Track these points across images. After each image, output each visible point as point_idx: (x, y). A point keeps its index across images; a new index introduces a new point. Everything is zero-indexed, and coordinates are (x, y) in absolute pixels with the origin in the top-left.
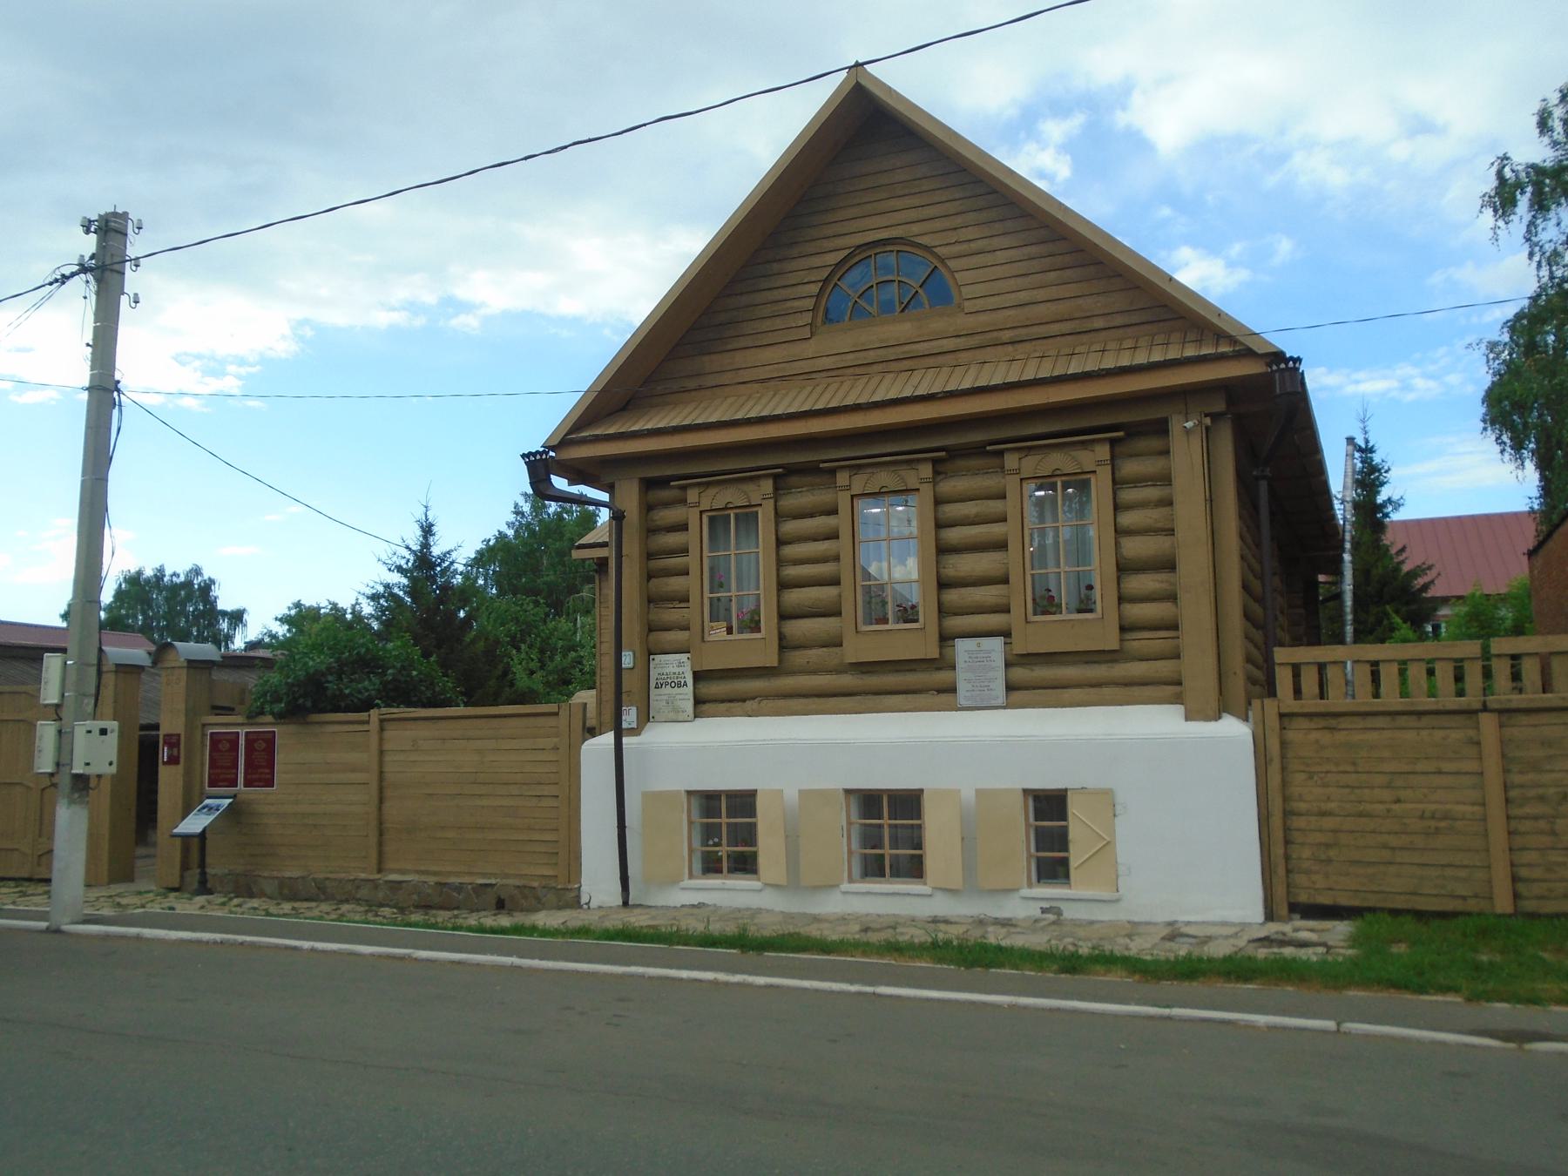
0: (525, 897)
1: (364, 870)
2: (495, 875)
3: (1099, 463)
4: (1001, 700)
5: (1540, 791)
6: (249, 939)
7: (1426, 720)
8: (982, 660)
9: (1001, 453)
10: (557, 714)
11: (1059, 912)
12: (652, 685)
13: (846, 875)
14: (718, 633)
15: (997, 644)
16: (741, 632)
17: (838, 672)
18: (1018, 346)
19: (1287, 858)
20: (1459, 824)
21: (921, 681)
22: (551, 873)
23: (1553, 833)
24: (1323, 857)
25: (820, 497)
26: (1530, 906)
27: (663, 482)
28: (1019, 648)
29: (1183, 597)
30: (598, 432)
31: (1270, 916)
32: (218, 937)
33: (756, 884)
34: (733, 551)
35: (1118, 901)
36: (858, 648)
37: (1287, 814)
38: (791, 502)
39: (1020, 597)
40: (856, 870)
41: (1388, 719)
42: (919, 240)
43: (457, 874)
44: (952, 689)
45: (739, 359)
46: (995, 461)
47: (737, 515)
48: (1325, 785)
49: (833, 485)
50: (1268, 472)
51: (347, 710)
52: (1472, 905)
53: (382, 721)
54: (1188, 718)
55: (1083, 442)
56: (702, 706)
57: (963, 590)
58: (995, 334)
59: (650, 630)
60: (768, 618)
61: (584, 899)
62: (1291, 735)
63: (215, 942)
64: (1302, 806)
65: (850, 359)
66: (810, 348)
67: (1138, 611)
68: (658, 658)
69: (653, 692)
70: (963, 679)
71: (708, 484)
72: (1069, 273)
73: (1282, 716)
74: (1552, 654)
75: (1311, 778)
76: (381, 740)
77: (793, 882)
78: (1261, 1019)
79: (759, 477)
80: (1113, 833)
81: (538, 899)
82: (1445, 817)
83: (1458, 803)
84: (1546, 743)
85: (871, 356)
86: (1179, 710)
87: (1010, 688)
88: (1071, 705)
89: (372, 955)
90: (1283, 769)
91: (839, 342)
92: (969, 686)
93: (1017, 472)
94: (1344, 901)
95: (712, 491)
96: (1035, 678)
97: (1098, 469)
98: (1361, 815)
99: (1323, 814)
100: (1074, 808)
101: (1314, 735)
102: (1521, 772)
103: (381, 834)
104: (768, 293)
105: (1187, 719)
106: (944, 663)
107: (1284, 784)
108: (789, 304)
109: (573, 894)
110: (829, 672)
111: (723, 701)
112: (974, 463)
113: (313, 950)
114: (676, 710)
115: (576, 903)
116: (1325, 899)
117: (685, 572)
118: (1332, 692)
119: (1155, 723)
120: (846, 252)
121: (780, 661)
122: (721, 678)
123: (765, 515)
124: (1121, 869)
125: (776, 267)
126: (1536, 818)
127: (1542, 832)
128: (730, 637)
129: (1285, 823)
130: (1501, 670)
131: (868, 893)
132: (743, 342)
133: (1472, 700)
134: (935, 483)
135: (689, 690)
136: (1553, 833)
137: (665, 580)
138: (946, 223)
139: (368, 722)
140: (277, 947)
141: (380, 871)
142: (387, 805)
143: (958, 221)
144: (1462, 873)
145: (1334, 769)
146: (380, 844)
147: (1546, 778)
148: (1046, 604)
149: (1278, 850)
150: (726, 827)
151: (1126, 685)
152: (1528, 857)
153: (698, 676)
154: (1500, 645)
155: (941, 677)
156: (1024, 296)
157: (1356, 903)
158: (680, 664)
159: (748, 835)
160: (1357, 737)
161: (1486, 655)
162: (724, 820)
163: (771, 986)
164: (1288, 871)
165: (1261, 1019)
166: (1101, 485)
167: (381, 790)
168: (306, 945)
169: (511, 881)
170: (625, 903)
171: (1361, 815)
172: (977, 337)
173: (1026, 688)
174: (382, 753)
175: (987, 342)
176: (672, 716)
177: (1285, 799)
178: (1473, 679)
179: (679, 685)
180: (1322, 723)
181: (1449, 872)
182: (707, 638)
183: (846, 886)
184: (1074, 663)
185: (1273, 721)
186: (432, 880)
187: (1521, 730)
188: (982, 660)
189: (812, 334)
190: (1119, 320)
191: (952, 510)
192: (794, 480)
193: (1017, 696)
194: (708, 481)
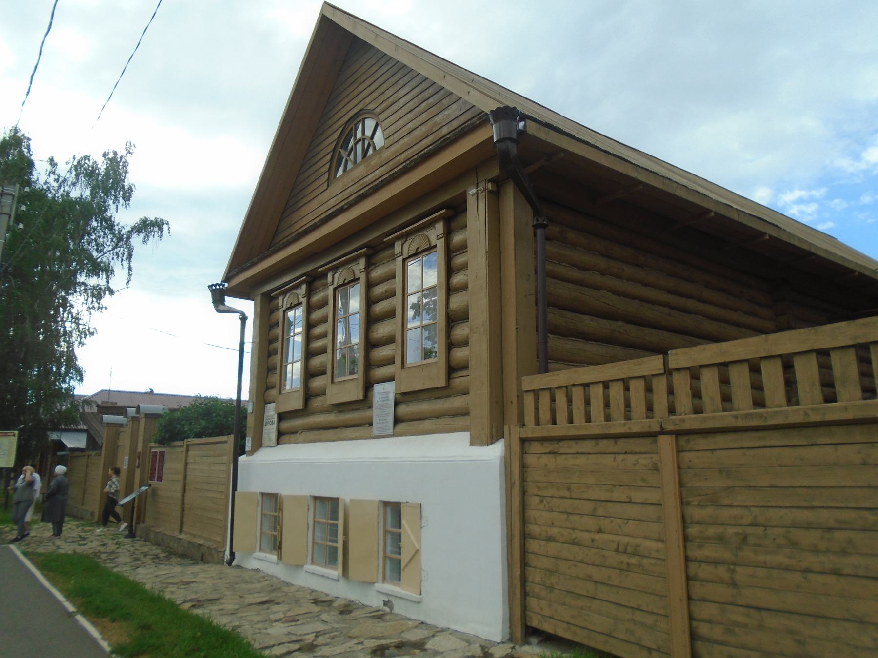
4: (390, 431)
5: (720, 530)
7: (622, 444)
9: (391, 245)
10: (226, 442)
11: (391, 608)
13: (258, 546)
20: (645, 561)
23: (734, 584)
35: (419, 603)
48: (551, 510)
58: (398, 158)
74: (702, 366)
83: (645, 537)
84: (725, 472)
88: (315, 441)
99: (550, 539)
101: (545, 459)
102: (700, 506)
106: (366, 401)
108: (317, 173)
114: (270, 440)
126: (716, 563)
127: (721, 582)
135: (275, 426)
136: (734, 584)
142: (187, 493)
145: (556, 494)
147: (725, 513)
151: (437, 417)
154: (680, 357)
157: (568, 636)
159: (277, 523)
160: (571, 461)
167: (185, 485)
172: (391, 163)
174: (186, 464)
181: (639, 616)
185: (516, 447)
187: (699, 455)
193: (401, 427)
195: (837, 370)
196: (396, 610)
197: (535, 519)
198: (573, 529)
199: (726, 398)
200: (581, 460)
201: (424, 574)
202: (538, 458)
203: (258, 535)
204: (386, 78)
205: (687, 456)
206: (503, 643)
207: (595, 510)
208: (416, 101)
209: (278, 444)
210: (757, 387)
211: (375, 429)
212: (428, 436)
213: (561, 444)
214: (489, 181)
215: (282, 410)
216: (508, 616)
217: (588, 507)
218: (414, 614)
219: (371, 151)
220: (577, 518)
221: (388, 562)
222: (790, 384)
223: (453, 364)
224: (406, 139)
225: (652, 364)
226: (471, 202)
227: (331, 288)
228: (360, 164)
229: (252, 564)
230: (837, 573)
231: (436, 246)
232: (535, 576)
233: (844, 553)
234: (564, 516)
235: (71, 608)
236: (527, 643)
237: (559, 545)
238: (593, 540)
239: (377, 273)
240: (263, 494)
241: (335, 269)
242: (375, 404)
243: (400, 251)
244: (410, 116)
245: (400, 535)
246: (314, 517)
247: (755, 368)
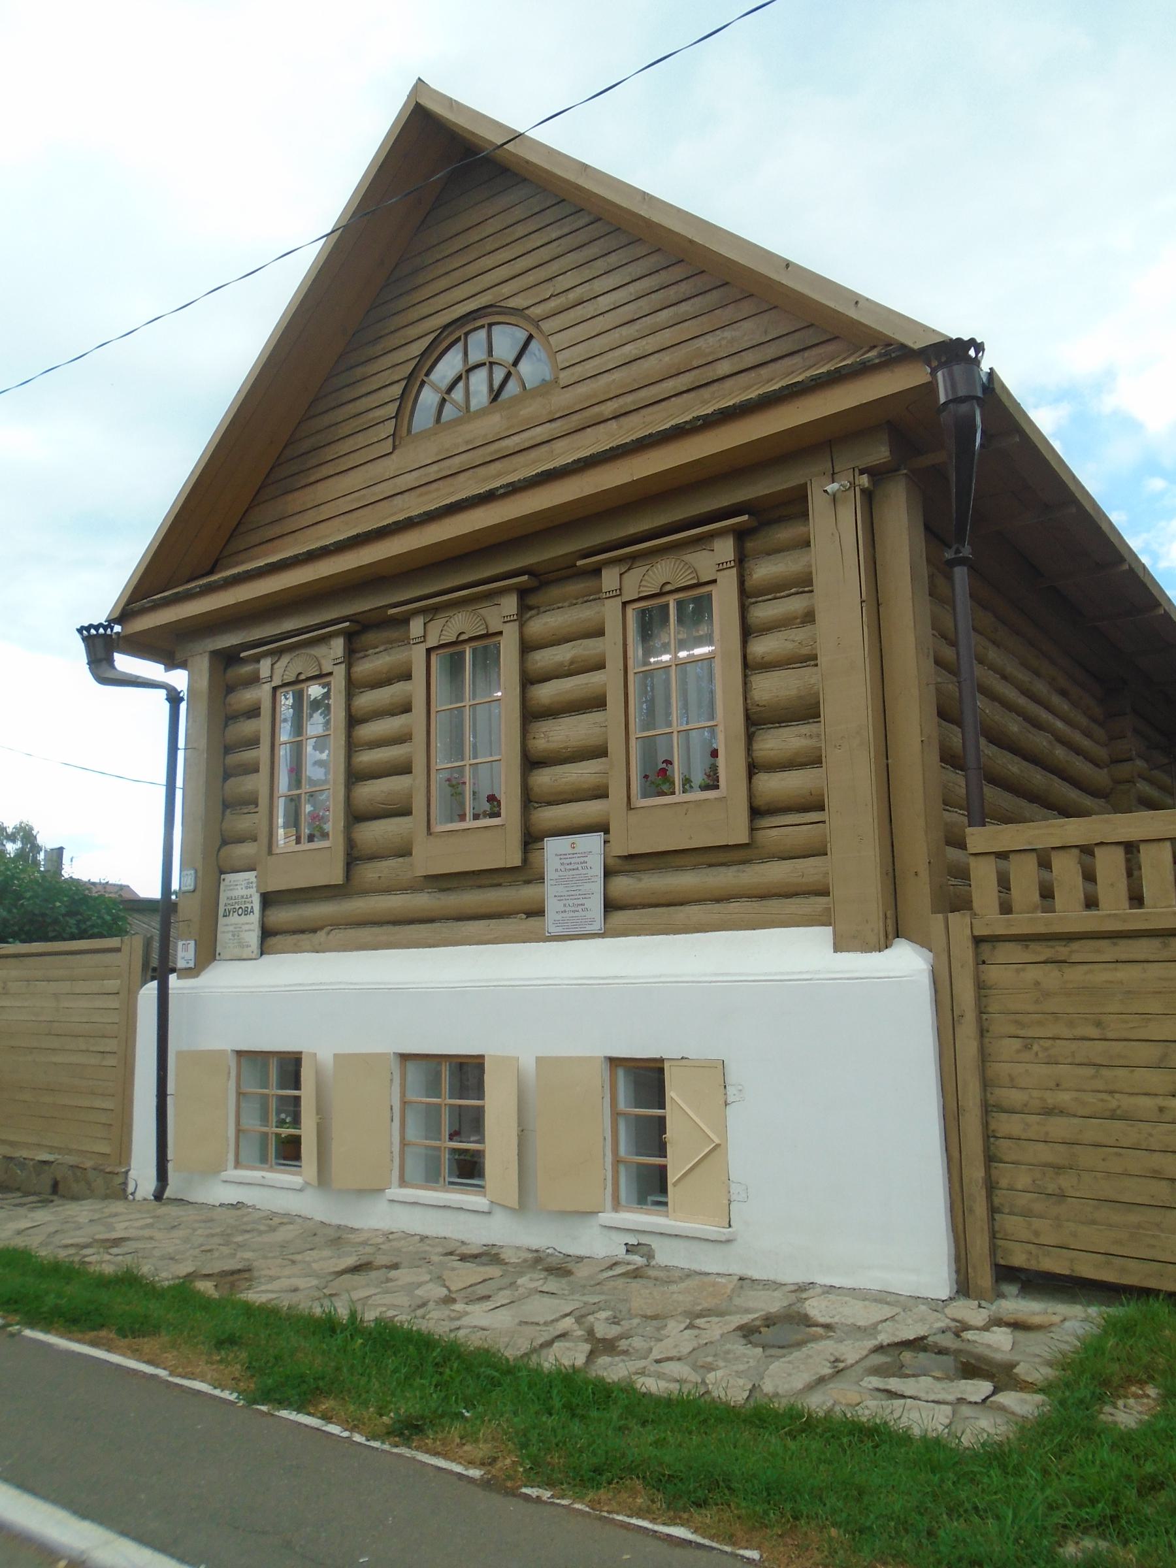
2: (59, 1150)
3: (721, 567)
8: (573, 866)
9: (596, 571)
10: (118, 950)
11: (650, 1255)
15: (593, 843)
16: (476, 817)
18: (623, 420)
19: (991, 1187)
21: (494, 899)
24: (1051, 1188)
25: (582, 615)
28: (619, 849)
29: (832, 757)
31: (964, 1288)
34: (467, 703)
35: (728, 1241)
36: (431, 857)
37: (988, 1109)
38: (540, 625)
39: (619, 772)
40: (415, 1167)
41: (1156, 943)
42: (511, 303)
44: (538, 912)
45: (323, 491)
47: (680, 604)
48: (1052, 1062)
49: (596, 596)
50: (966, 551)
54: (839, 946)
58: (596, 409)
59: (225, 842)
60: (731, 768)
61: (130, 1189)
62: (993, 974)
64: (1014, 1097)
65: (433, 472)
67: (773, 785)
68: (230, 878)
70: (553, 894)
71: (633, 558)
72: (685, 307)
73: (978, 941)
75: (1028, 1047)
77: (524, 1203)
80: (723, 1130)
86: (825, 934)
88: (375, 948)
90: (982, 1032)
94: (1087, 1270)
96: (646, 891)
97: (720, 577)
99: (1049, 1112)
101: (1033, 973)
105: (837, 948)
106: (527, 871)
107: (984, 1057)
108: (371, 415)
109: (120, 1180)
114: (242, 945)
117: (598, 703)
119: (794, 954)
121: (525, 860)
122: (294, 902)
129: (986, 1125)
135: (255, 918)
138: (542, 274)
143: (554, 267)
145: (1066, 1032)
148: (659, 779)
149: (976, 1173)
150: (279, 1096)
151: (718, 900)
153: (268, 900)
156: (630, 350)
159: (470, 1122)
160: (1101, 976)
164: (993, 1210)
170: (159, 1196)
171: (1113, 1116)
172: (575, 417)
173: (634, 907)
177: (986, 1084)
180: (1044, 951)
183: (395, 1192)
185: (964, 951)
189: (394, 448)
190: (750, 359)
191: (544, 659)
192: (370, 637)
193: (619, 918)
196: (661, 1259)
197: (1012, 1079)
198: (1111, 1092)
199: (1047, 893)
201: (734, 1188)
202: (1018, 971)
203: (396, 1148)
204: (560, 250)
206: (951, 1299)
207: (1165, 1056)
208: (644, 305)
209: (262, 954)
211: (552, 920)
212: (671, 937)
213: (1075, 946)
214: (862, 472)
215: (277, 883)
216: (953, 1252)
217: (1148, 1053)
218: (710, 1262)
219: (512, 388)
220: (1121, 1072)
221: (622, 1169)
223: (760, 802)
224: (616, 376)
226: (818, 503)
227: (267, 688)
228: (482, 413)
229: (220, 1192)
231: (331, 674)
232: (1017, 1178)
234: (1091, 1071)
236: (1001, 1295)
237: (1075, 1121)
238: (1161, 1109)
239: (764, 571)
240: (239, 1054)
241: (432, 612)
242: (550, 873)
243: (268, 674)
244: (627, 331)
245: (662, 1121)
246: (403, 1094)
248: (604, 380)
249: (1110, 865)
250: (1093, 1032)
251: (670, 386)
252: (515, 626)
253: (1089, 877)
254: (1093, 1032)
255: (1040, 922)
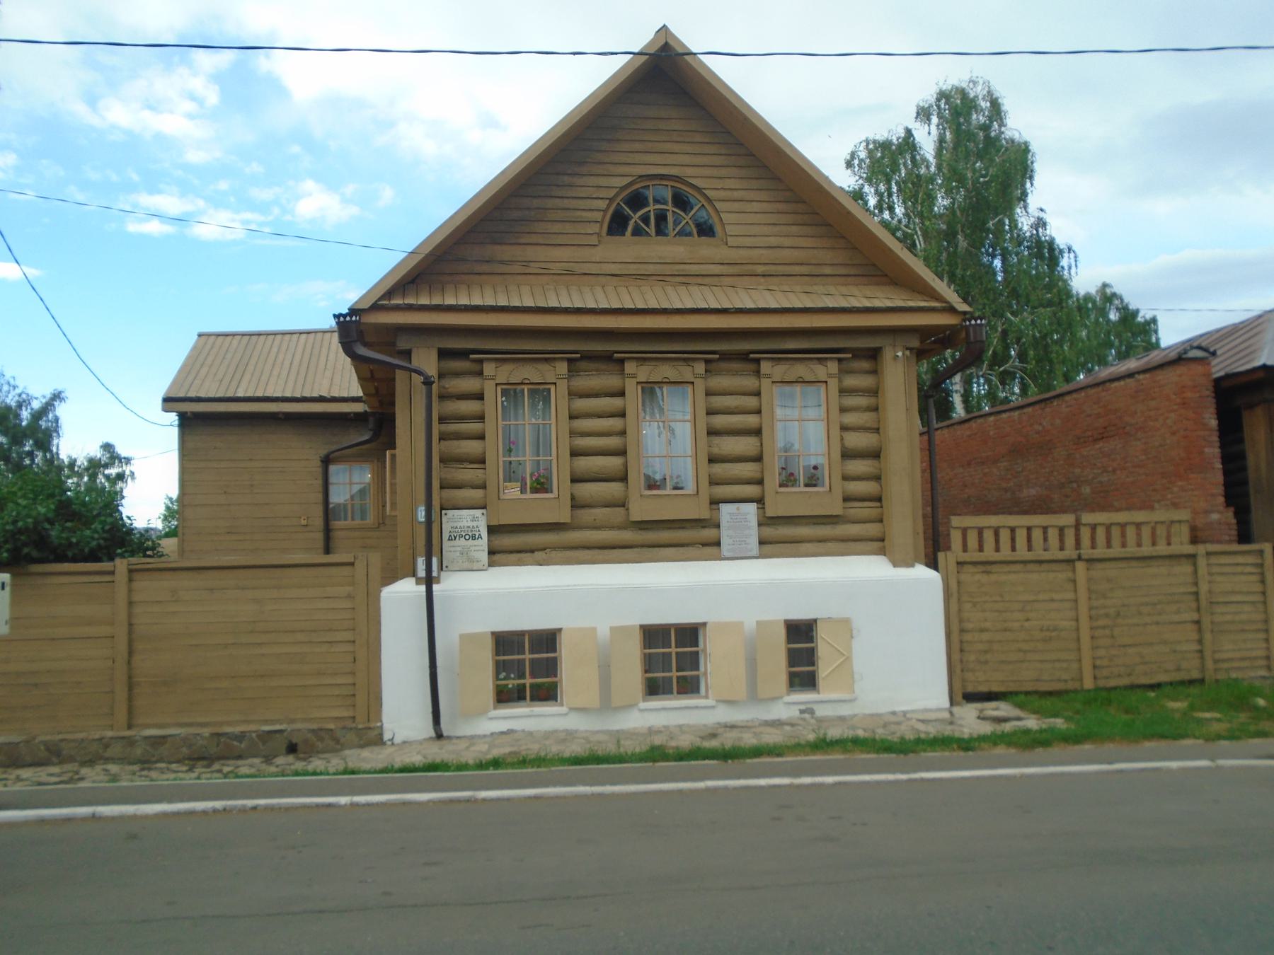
0: (321, 739)
1: (112, 727)
3: (830, 376)
6: (262, 802)
7: (1045, 566)
8: (739, 520)
11: (811, 712)
12: (445, 536)
14: (513, 491)
15: (751, 508)
17: (619, 528)
21: (692, 536)
22: (345, 714)
23: (1113, 637)
25: (612, 381)
26: (1101, 683)
27: (463, 354)
30: (410, 300)
32: (218, 804)
33: (564, 709)
35: (850, 701)
36: (642, 508)
42: (693, 181)
43: (229, 723)
46: (752, 366)
48: (984, 611)
51: (74, 560)
52: (1070, 686)
53: (130, 571)
55: (818, 359)
56: (496, 555)
57: (724, 465)
61: (387, 736)
63: (215, 811)
64: (969, 626)
65: (632, 269)
66: (597, 254)
68: (450, 513)
69: (446, 544)
73: (958, 563)
76: (130, 591)
78: (1174, 765)
79: (554, 359)
80: (850, 649)
81: (337, 741)
82: (1055, 630)
85: (651, 269)
87: (762, 542)
89: (429, 801)
91: (627, 250)
92: (731, 541)
93: (493, 378)
94: (996, 688)
95: (507, 368)
96: (780, 535)
98: (1006, 630)
99: (982, 630)
100: (822, 633)
101: (978, 577)
103: (131, 687)
104: (557, 201)
108: (579, 213)
109: (376, 732)
110: (612, 528)
111: (511, 552)
112: (735, 366)
113: (353, 805)
114: (471, 560)
115: (378, 741)
116: (983, 688)
118: (1174, 540)
120: (630, 179)
122: (512, 532)
123: (559, 394)
124: (856, 676)
125: (566, 179)
126: (1104, 627)
128: (524, 496)
130: (1085, 534)
131: (664, 709)
132: (534, 239)
133: (1070, 552)
134: (569, 378)
137: (456, 443)
138: (714, 172)
139: (113, 573)
140: (305, 806)
141: (130, 727)
143: (724, 172)
144: (1065, 665)
146: (130, 699)
148: (789, 480)
150: (527, 663)
151: (843, 541)
152: (1102, 652)
153: (492, 530)
154: (1088, 518)
155: (708, 533)
157: (1002, 689)
158: (474, 519)
161: (1078, 525)
162: (528, 656)
163: (840, 783)
165: (1174, 765)
166: (559, 394)
168: (343, 800)
169: (298, 726)
170: (439, 736)
171: (1006, 630)
173: (771, 543)
175: (745, 273)
176: (467, 565)
177: (961, 621)
178: (1116, 540)
179: (474, 537)
180: (981, 568)
182: (502, 497)
183: (642, 705)
184: (807, 524)
186: (206, 732)
188: (739, 520)
192: (583, 365)
193: (497, 557)
194: (504, 357)
195: (1158, 532)
200: (1012, 577)
205: (963, 577)
210: (1013, 540)
218: (845, 711)
222: (1093, 539)
225: (1067, 519)
226: (888, 354)
230: (1157, 623)
233: (1160, 614)
235: (1221, 762)
247: (1045, 529)
248: (757, 252)
249: (1005, 536)
250: (998, 598)
251: (797, 269)
252: (836, 380)
253: (1045, 539)
254: (998, 598)
255: (978, 557)
